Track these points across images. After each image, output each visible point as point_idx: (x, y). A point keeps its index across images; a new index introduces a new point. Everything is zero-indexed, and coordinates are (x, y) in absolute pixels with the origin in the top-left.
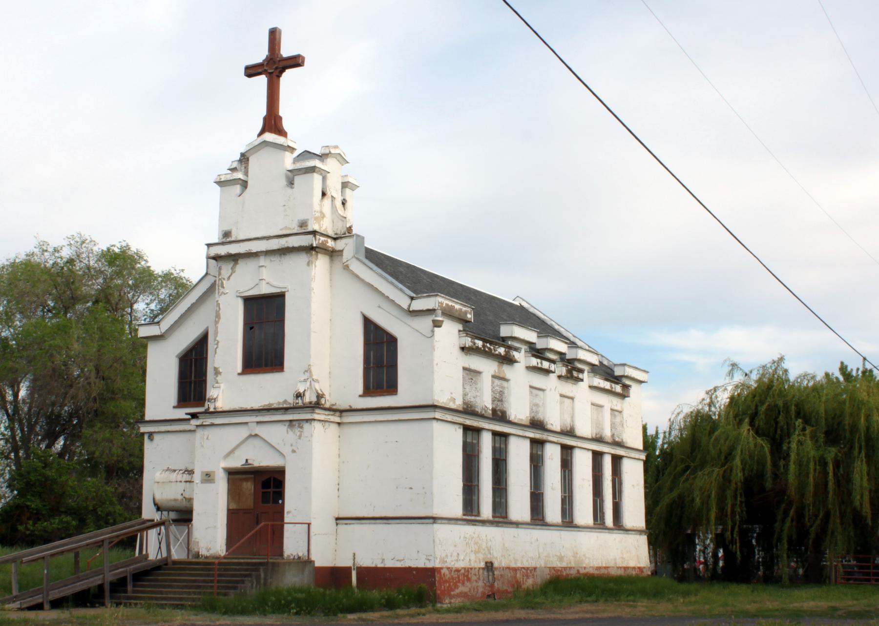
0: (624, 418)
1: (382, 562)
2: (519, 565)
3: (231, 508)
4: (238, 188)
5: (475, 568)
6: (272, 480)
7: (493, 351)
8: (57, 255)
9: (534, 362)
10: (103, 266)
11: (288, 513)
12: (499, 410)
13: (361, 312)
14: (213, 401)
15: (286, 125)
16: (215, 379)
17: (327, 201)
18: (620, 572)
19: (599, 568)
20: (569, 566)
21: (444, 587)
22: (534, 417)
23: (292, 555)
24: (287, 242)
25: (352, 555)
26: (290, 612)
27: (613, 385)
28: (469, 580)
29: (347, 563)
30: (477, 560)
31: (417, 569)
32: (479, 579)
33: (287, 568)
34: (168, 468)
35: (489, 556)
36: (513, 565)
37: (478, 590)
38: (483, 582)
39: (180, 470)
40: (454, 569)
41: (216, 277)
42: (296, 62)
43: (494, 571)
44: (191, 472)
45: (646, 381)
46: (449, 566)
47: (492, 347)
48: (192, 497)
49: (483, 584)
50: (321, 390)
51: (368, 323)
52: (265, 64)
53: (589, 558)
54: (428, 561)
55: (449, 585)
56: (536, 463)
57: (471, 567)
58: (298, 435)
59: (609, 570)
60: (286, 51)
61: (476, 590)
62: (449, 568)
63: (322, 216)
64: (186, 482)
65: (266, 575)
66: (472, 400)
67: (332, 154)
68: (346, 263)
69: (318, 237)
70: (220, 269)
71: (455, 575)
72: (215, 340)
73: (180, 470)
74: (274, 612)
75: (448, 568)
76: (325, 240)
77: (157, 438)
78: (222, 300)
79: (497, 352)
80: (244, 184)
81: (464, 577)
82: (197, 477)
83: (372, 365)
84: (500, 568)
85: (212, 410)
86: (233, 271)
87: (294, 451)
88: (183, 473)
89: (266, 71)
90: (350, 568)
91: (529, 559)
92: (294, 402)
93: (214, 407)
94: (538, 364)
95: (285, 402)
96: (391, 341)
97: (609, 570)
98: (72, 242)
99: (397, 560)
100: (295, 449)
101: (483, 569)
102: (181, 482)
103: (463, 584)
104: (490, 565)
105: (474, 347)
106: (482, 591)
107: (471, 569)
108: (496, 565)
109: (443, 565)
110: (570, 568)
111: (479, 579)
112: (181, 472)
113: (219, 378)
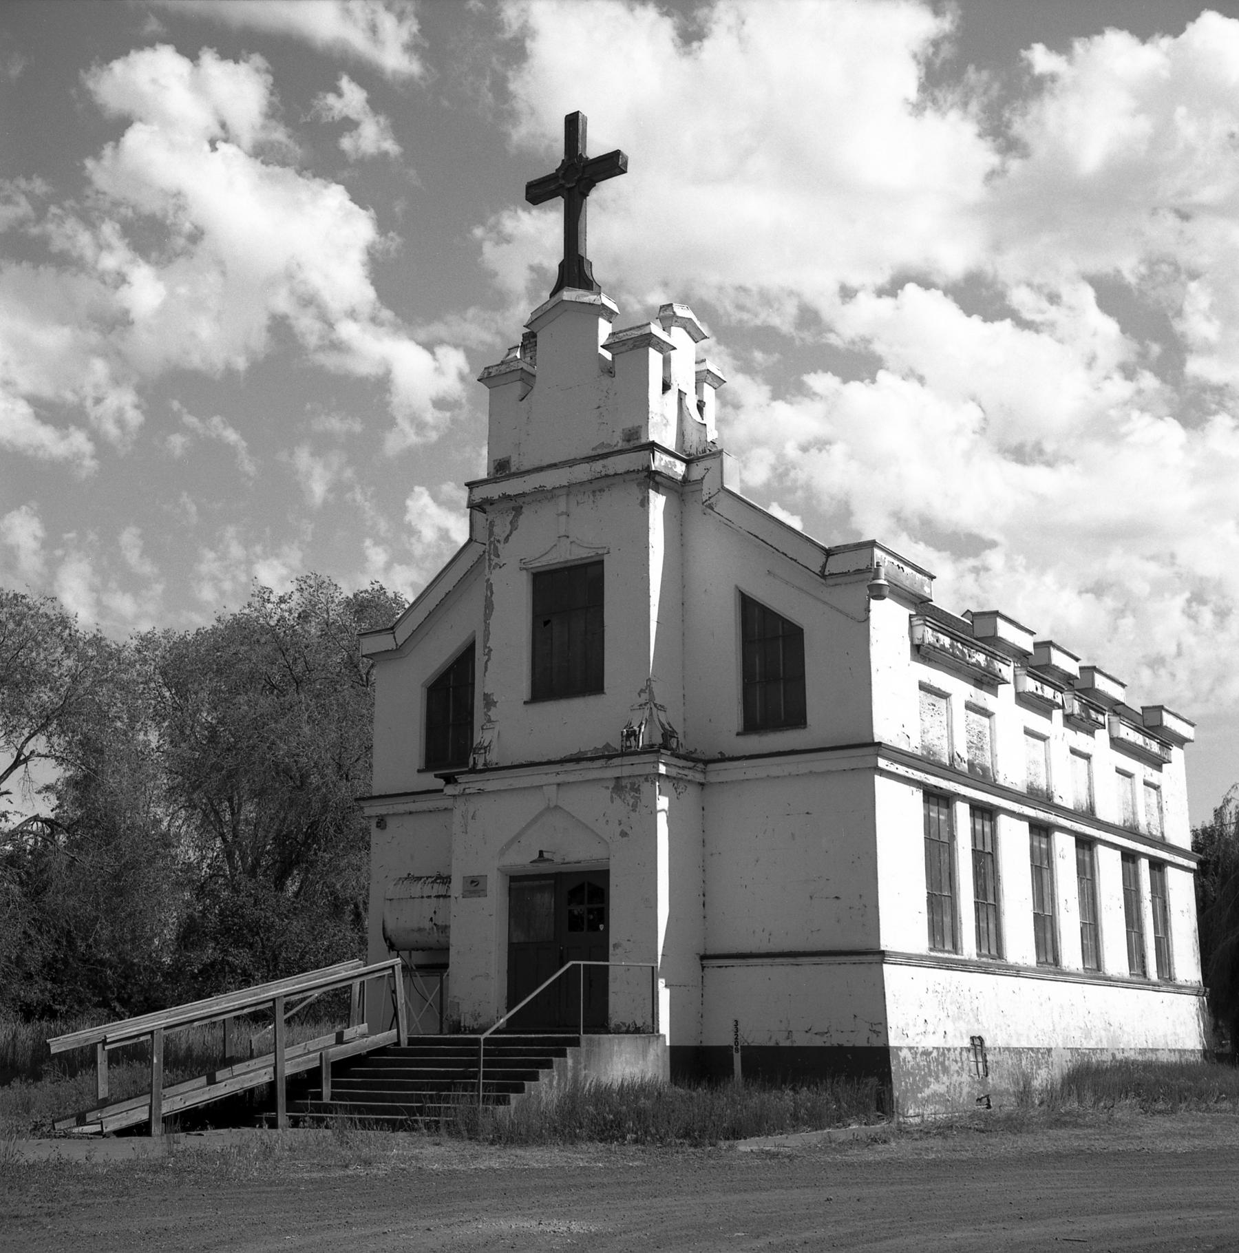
0: (1163, 798)
1: (788, 1038)
2: (1024, 1044)
3: (515, 941)
4: (517, 388)
5: (955, 1049)
6: (586, 885)
7: (968, 658)
8: (283, 606)
9: (1030, 685)
10: (348, 620)
11: (615, 946)
12: (979, 764)
13: (737, 587)
14: (482, 751)
15: (598, 273)
16: (486, 714)
17: (672, 395)
18: (1174, 1058)
19: (1143, 1051)
20: (1100, 1047)
21: (906, 1083)
22: (1032, 783)
23: (624, 1024)
24: (604, 466)
25: (732, 1024)
26: (624, 1138)
27: (1148, 740)
28: (946, 1070)
29: (726, 1039)
30: (958, 1035)
31: (854, 1050)
32: (962, 1068)
33: (616, 1048)
34: (409, 874)
35: (976, 1026)
36: (1014, 1044)
37: (961, 1089)
38: (970, 1076)
39: (427, 878)
40: (920, 1050)
41: (485, 544)
42: (613, 164)
43: (985, 1055)
44: (445, 880)
45: (1192, 738)
46: (911, 1045)
47: (966, 651)
48: (448, 924)
49: (969, 1079)
50: (669, 724)
51: (747, 604)
52: (560, 175)
53: (1129, 1034)
54: (875, 1035)
55: (914, 1080)
56: (1042, 866)
57: (948, 1046)
58: (631, 804)
59: (1159, 1054)
60: (596, 145)
61: (958, 1089)
62: (913, 1048)
63: (665, 422)
64: (438, 897)
65: (577, 1062)
66: (936, 742)
67: (678, 317)
68: (708, 502)
69: (657, 454)
70: (492, 524)
71: (922, 1061)
72: (485, 647)
73: (427, 878)
74: (591, 1139)
75: (910, 1048)
76: (670, 462)
77: (392, 824)
78: (496, 577)
79: (974, 660)
80: (528, 379)
81: (937, 1066)
82: (456, 887)
83: (758, 679)
84: (995, 1049)
85: (480, 766)
86: (514, 525)
87: (624, 834)
88: (432, 882)
89: (562, 186)
90: (729, 1048)
91: (1039, 1033)
92: (622, 746)
93: (483, 762)
94: (1037, 689)
95: (607, 746)
96: (792, 636)
97: (1159, 1054)
98: (303, 586)
99: (816, 1034)
100: (627, 829)
101: (968, 1050)
102: (429, 897)
103: (937, 1079)
104: (977, 1042)
105: (938, 645)
106: (969, 1093)
107: (949, 1050)
108: (988, 1044)
109: (901, 1042)
110: (1102, 1050)
111: (962, 1068)
112: (430, 880)
113: (493, 713)
